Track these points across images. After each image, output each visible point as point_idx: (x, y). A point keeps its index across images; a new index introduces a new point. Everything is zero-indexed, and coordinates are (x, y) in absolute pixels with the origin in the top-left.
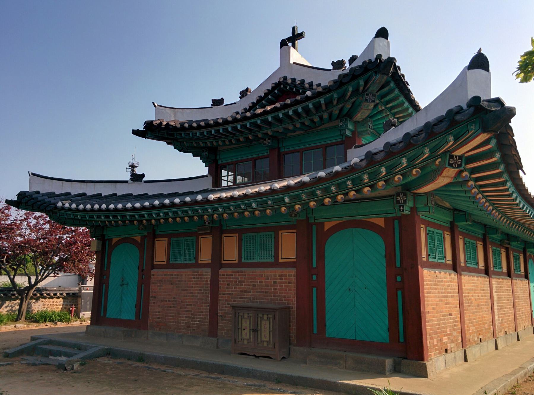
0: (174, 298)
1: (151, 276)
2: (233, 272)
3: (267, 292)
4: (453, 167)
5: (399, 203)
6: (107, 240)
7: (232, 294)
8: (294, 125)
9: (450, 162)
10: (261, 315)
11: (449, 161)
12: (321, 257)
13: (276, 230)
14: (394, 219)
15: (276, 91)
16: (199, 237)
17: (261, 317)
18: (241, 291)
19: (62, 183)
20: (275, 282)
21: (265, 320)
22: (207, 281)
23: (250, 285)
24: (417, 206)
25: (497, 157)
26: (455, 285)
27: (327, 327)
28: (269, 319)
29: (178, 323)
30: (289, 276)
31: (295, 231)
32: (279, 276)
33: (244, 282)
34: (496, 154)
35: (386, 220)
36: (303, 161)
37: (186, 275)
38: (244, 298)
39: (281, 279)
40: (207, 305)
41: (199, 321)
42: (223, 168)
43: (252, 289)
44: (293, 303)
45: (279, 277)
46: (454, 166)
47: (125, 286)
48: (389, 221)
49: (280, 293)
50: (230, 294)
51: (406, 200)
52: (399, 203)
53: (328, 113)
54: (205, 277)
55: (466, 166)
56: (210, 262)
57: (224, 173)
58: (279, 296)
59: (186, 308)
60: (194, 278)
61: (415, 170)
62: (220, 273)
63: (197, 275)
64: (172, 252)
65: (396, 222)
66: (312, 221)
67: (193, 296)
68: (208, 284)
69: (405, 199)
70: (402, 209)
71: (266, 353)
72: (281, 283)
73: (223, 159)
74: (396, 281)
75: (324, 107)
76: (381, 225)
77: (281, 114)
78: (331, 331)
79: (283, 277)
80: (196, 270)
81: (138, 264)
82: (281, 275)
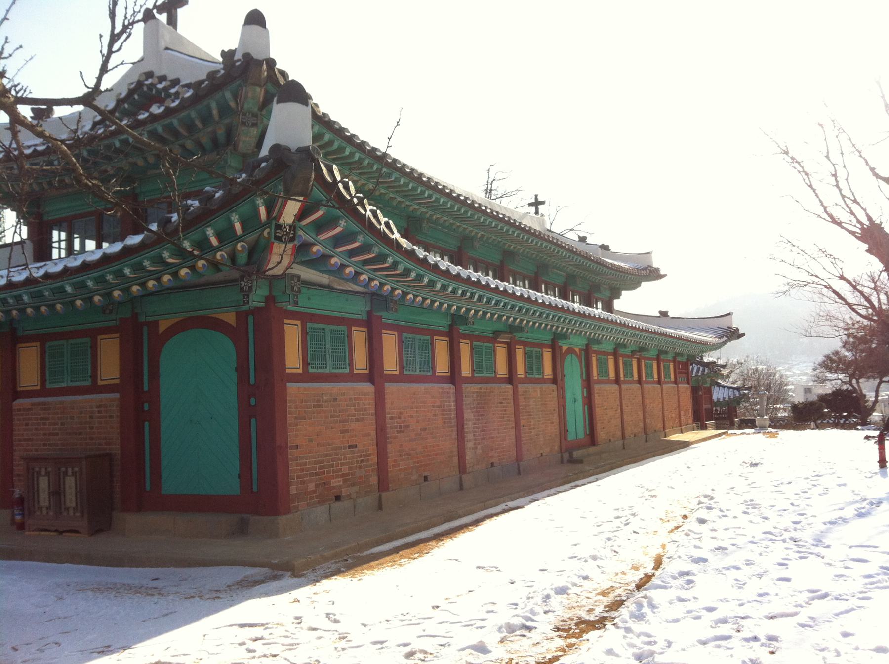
3: (80, 434)
4: (282, 241)
8: (145, 159)
9: (277, 234)
10: (63, 469)
11: (276, 233)
13: (93, 334)
15: (136, 97)
16: (97, 339)
18: (45, 434)
20: (91, 417)
22: (450, 406)
24: (274, 294)
25: (342, 226)
26: (369, 403)
27: (163, 480)
31: (117, 335)
32: (97, 407)
33: (48, 419)
34: (341, 222)
35: (239, 315)
39: (99, 412)
42: (54, 227)
44: (116, 449)
45: (96, 409)
46: (284, 240)
48: (242, 317)
50: (29, 440)
51: (251, 286)
53: (192, 140)
55: (318, 237)
56: (117, 382)
57: (55, 234)
61: (239, 245)
62: (14, 408)
64: (344, 346)
65: (251, 319)
66: (142, 319)
69: (250, 285)
73: (53, 211)
74: (250, 405)
75: (199, 124)
76: (230, 322)
78: (170, 486)
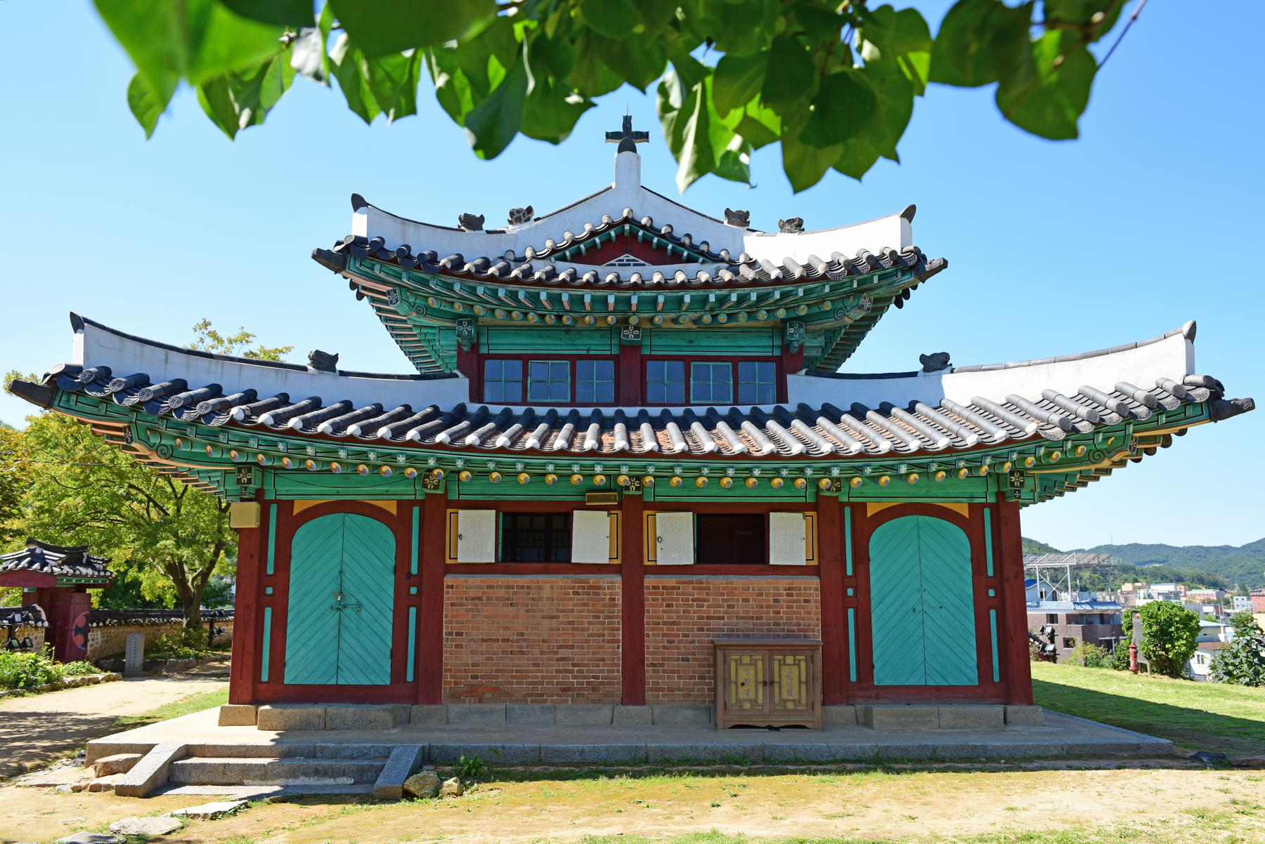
0: (523, 634)
1: (445, 590)
2: (679, 582)
3: (760, 618)
5: (1014, 486)
6: (271, 502)
7: (679, 623)
12: (862, 558)
14: (983, 506)
17: (780, 661)
19: (223, 363)
21: (789, 665)
23: (720, 606)
27: (875, 671)
28: (797, 662)
29: (535, 683)
30: (805, 589)
32: (785, 590)
35: (971, 506)
36: (691, 379)
37: (552, 588)
38: (708, 630)
40: (616, 645)
41: (597, 677)
43: (726, 613)
45: (785, 592)
47: (348, 611)
49: (787, 619)
50: (673, 623)
52: (1014, 486)
54: (606, 591)
58: (785, 624)
59: (556, 653)
60: (576, 593)
63: (583, 588)
67: (573, 629)
68: (616, 605)
70: (1017, 495)
71: (795, 720)
72: (790, 601)
77: (714, 295)
79: (794, 592)
80: (583, 577)
81: (391, 563)
82: (790, 589)
